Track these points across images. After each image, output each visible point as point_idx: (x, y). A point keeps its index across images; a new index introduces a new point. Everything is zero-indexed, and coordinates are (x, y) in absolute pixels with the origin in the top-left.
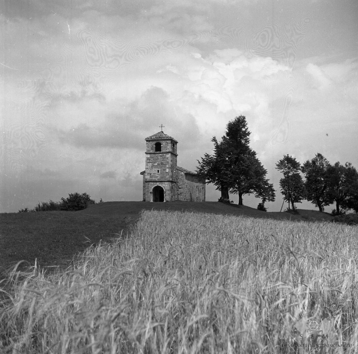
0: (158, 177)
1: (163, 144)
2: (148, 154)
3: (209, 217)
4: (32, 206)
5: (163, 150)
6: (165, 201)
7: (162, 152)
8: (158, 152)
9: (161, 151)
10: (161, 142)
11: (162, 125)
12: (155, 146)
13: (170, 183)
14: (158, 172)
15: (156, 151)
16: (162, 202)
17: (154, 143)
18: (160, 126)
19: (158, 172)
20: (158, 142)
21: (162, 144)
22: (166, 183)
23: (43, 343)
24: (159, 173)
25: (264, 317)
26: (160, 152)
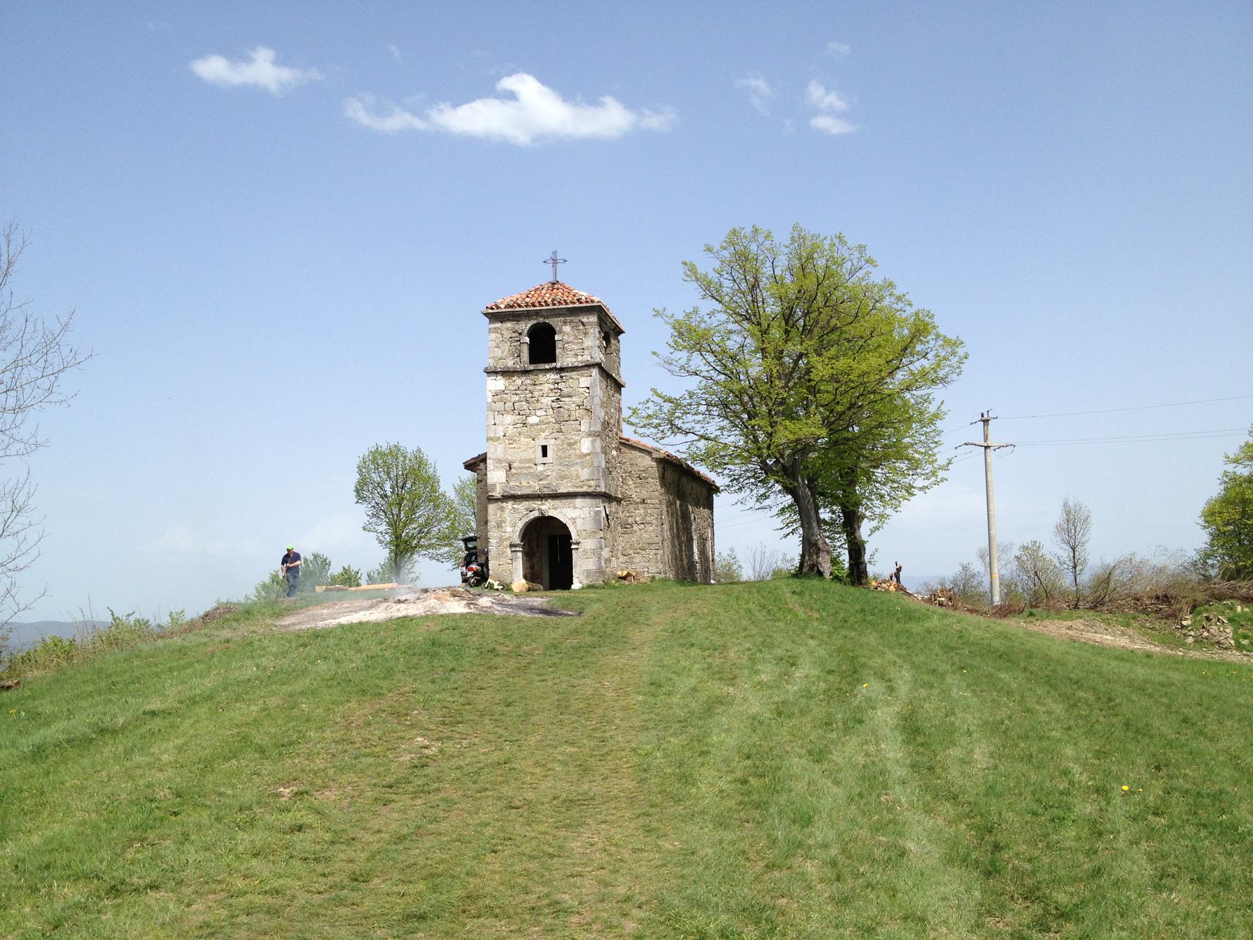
0: (552, 474)
1: (565, 333)
2: (496, 373)
3: (136, 663)
4: (196, 608)
5: (564, 359)
6: (576, 585)
7: (559, 365)
8: (542, 366)
9: (554, 360)
10: (554, 322)
11: (555, 253)
12: (527, 340)
13: (599, 501)
14: (545, 454)
15: (534, 359)
16: (565, 593)
17: (525, 326)
18: (548, 256)
19: (545, 454)
20: (541, 320)
21: (561, 332)
22: (579, 502)
23: (1108, 637)
24: (549, 459)
25: (926, 483)
26: (554, 365)
